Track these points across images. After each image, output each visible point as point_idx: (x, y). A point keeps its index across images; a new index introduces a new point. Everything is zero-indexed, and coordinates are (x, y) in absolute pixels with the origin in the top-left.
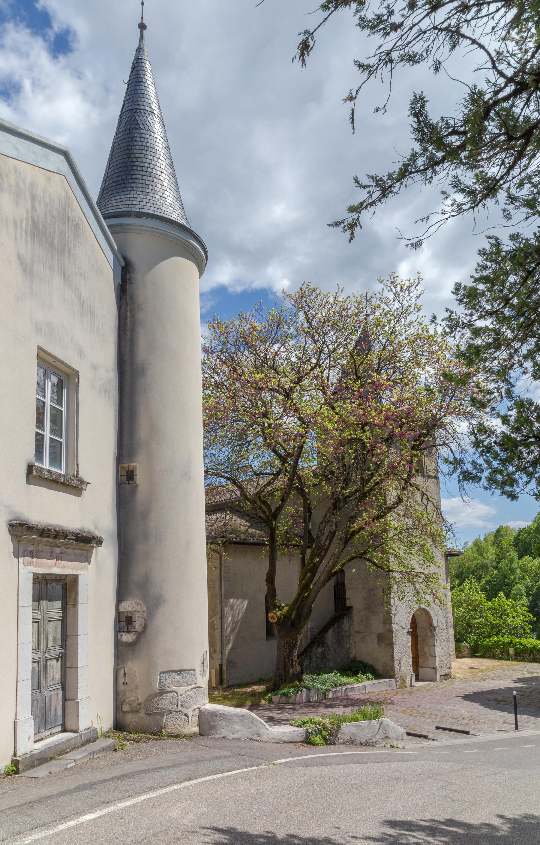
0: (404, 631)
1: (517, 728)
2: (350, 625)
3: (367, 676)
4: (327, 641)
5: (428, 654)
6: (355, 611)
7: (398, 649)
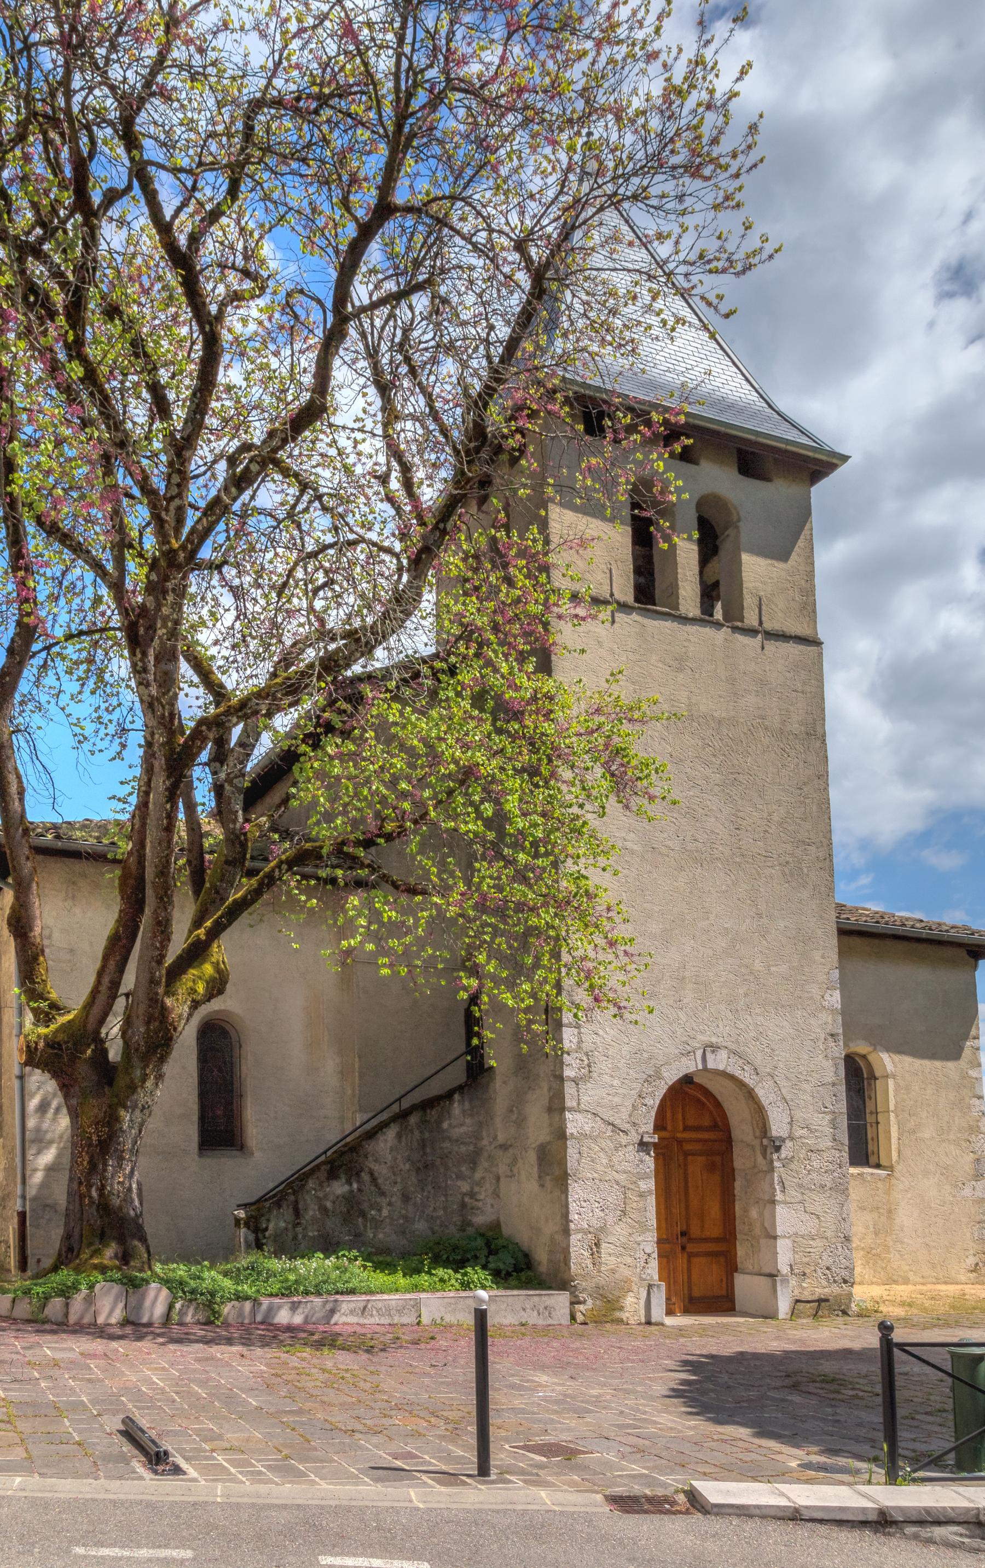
0: (623, 1139)
1: (483, 1470)
2: (480, 1124)
3: (465, 1274)
5: (757, 1231)
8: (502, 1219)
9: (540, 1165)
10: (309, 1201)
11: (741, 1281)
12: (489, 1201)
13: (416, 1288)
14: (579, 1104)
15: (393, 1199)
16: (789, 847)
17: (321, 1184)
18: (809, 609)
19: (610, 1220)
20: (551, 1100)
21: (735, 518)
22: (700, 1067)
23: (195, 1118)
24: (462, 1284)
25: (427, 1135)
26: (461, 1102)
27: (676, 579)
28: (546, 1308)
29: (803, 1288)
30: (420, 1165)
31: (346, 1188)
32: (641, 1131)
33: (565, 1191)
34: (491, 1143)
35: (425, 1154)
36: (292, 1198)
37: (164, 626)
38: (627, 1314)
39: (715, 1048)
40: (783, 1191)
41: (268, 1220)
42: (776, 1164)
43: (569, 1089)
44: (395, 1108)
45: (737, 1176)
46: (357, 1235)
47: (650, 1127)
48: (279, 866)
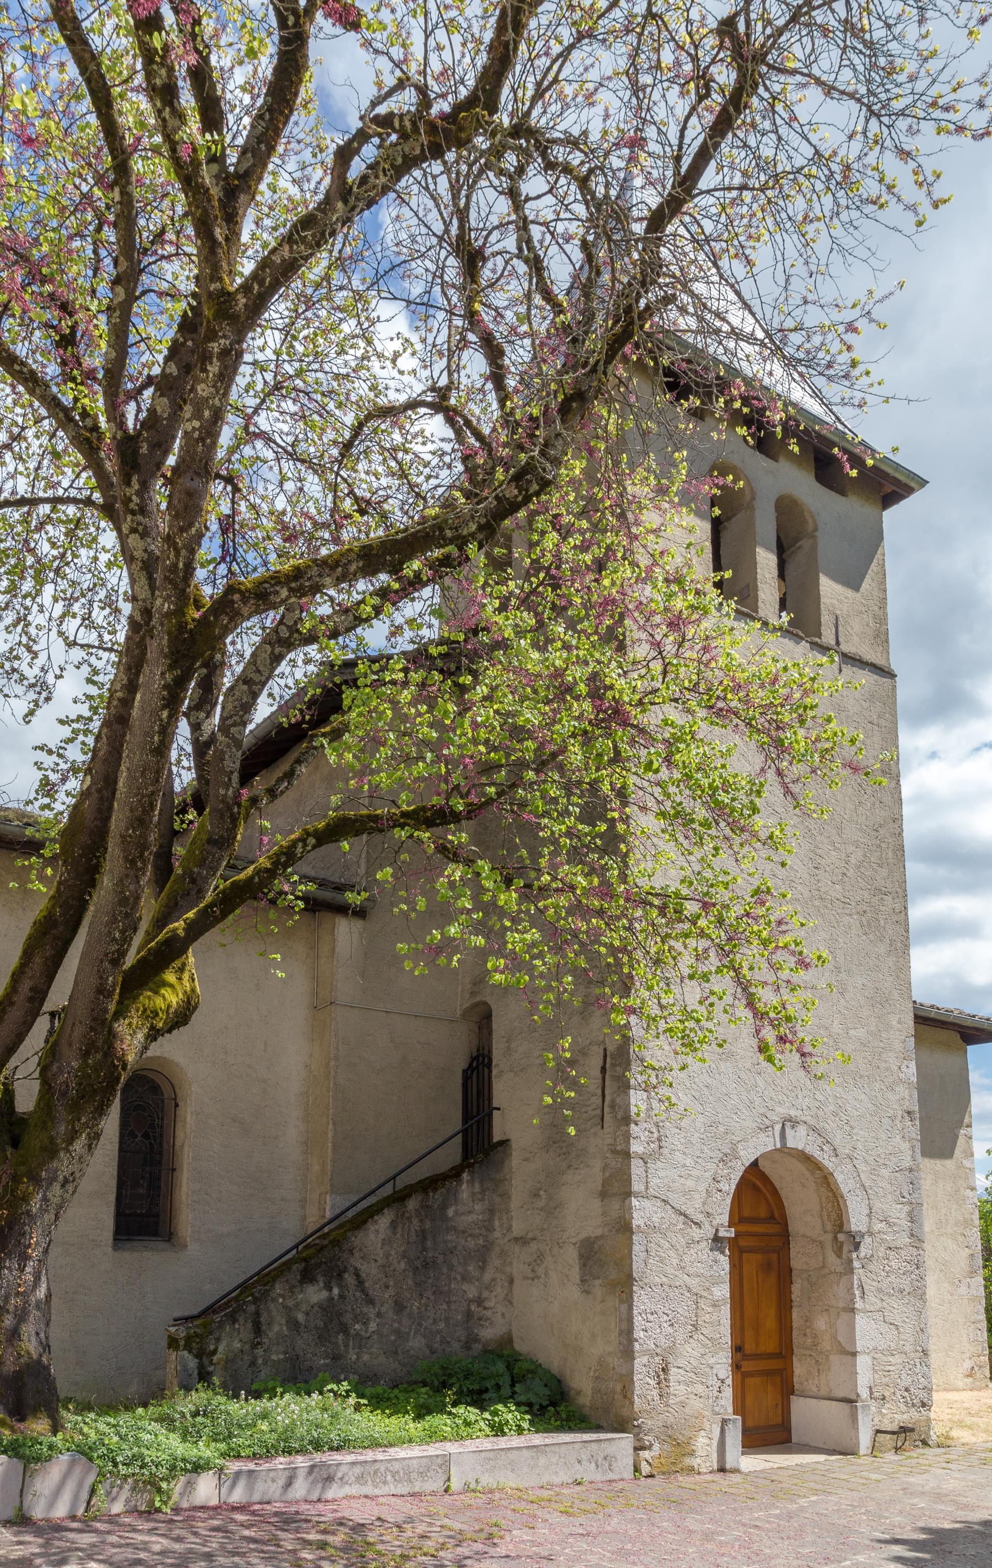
0: (696, 1233)
4: (356, 1261)
5: (826, 1344)
6: (515, 1159)
7: (659, 1308)
8: (515, 1334)
9: (583, 1266)
10: (274, 1313)
11: (799, 1406)
12: (500, 1309)
13: (433, 1436)
14: (647, 1188)
15: (384, 1309)
16: (866, 894)
17: (291, 1289)
18: (881, 638)
19: (680, 1337)
20: (606, 1182)
21: (810, 527)
22: (778, 1146)
23: (112, 1197)
24: (492, 1427)
25: (428, 1224)
26: (471, 1182)
27: (756, 579)
28: (605, 1458)
29: (883, 1415)
30: (418, 1263)
31: (325, 1294)
32: (715, 1223)
33: (628, 1301)
34: (504, 1235)
35: (425, 1249)
36: (252, 1308)
37: (197, 415)
38: (698, 1460)
39: (794, 1123)
40: (862, 1298)
41: (218, 1340)
42: (856, 1264)
43: (636, 1168)
44: (387, 1190)
45: (794, 1278)
46: (336, 1358)
47: (725, 1219)
48: (303, 840)
